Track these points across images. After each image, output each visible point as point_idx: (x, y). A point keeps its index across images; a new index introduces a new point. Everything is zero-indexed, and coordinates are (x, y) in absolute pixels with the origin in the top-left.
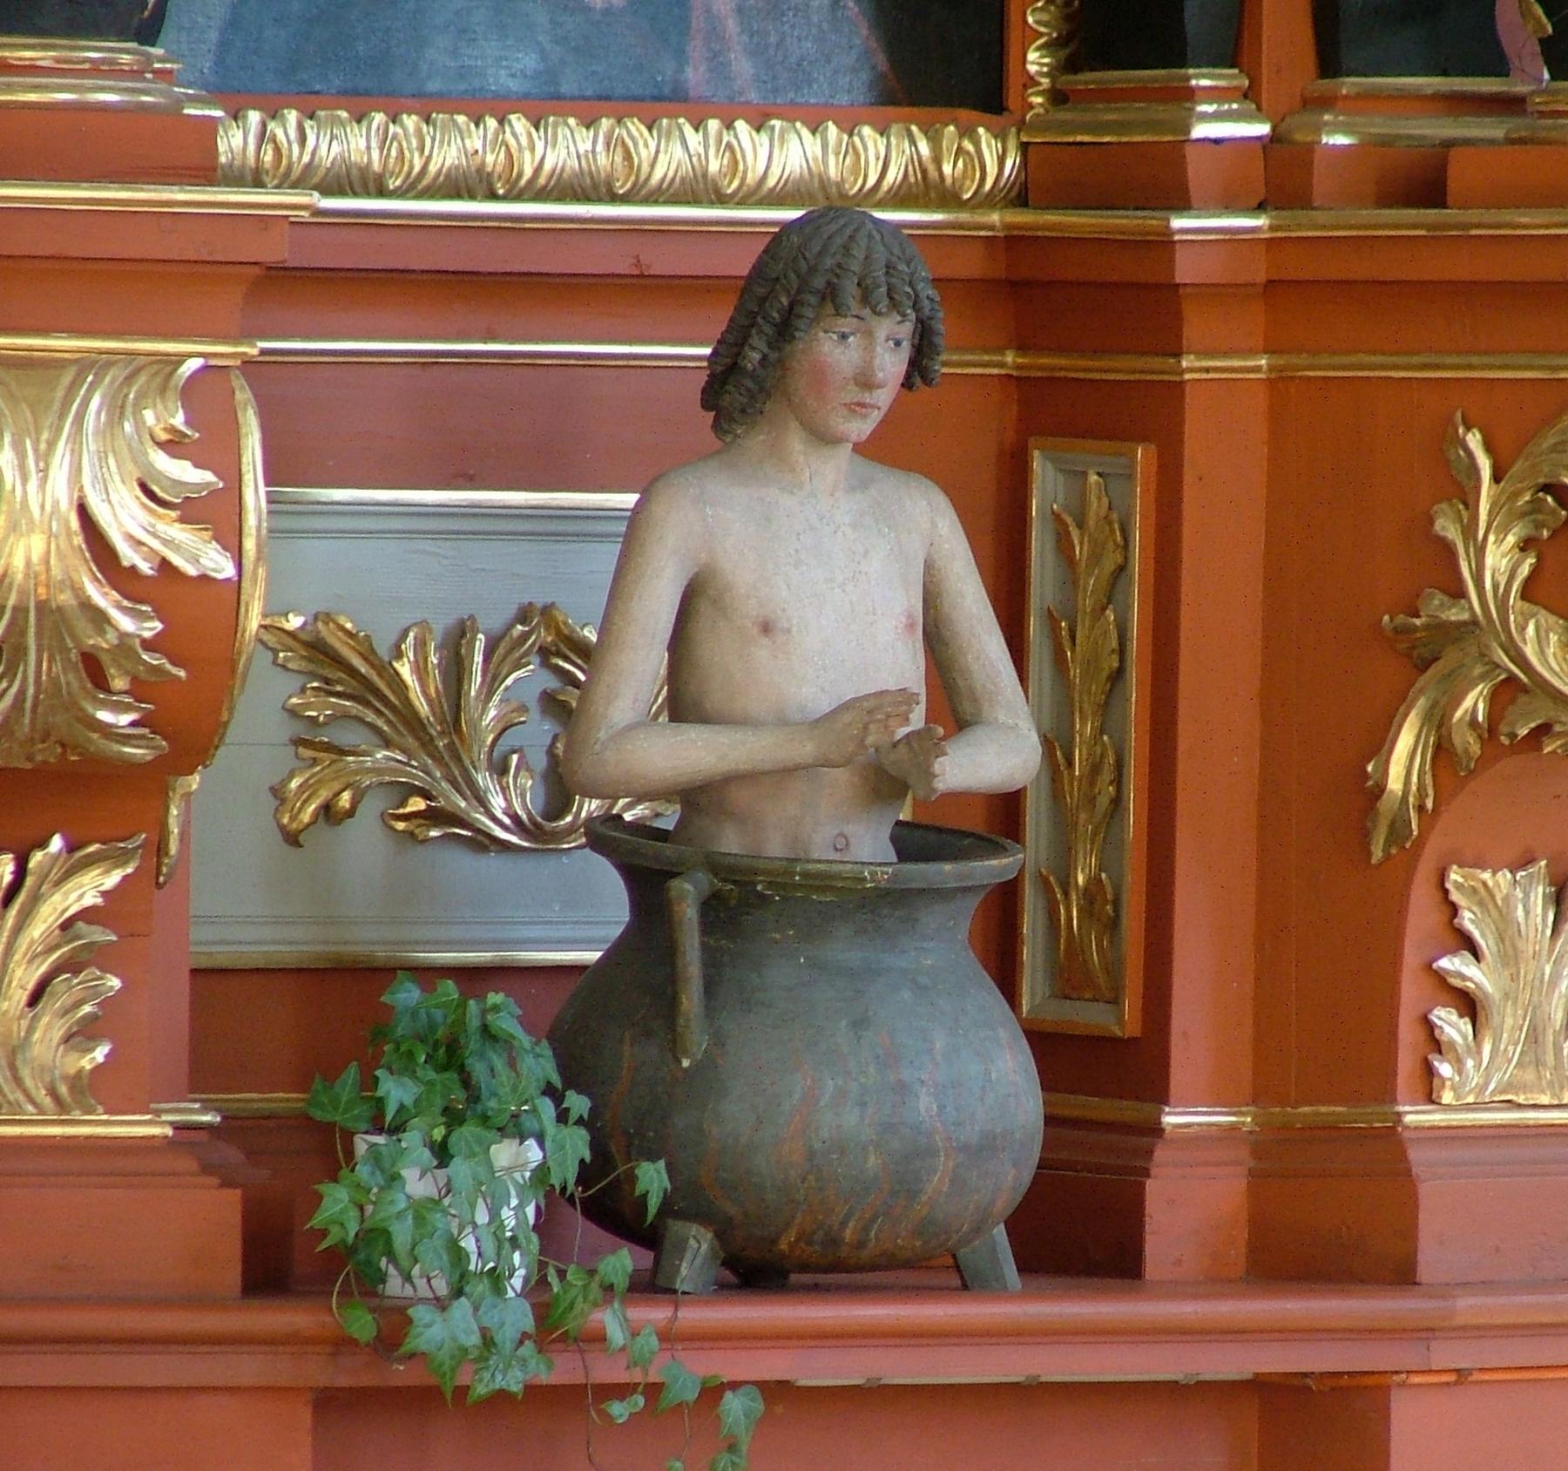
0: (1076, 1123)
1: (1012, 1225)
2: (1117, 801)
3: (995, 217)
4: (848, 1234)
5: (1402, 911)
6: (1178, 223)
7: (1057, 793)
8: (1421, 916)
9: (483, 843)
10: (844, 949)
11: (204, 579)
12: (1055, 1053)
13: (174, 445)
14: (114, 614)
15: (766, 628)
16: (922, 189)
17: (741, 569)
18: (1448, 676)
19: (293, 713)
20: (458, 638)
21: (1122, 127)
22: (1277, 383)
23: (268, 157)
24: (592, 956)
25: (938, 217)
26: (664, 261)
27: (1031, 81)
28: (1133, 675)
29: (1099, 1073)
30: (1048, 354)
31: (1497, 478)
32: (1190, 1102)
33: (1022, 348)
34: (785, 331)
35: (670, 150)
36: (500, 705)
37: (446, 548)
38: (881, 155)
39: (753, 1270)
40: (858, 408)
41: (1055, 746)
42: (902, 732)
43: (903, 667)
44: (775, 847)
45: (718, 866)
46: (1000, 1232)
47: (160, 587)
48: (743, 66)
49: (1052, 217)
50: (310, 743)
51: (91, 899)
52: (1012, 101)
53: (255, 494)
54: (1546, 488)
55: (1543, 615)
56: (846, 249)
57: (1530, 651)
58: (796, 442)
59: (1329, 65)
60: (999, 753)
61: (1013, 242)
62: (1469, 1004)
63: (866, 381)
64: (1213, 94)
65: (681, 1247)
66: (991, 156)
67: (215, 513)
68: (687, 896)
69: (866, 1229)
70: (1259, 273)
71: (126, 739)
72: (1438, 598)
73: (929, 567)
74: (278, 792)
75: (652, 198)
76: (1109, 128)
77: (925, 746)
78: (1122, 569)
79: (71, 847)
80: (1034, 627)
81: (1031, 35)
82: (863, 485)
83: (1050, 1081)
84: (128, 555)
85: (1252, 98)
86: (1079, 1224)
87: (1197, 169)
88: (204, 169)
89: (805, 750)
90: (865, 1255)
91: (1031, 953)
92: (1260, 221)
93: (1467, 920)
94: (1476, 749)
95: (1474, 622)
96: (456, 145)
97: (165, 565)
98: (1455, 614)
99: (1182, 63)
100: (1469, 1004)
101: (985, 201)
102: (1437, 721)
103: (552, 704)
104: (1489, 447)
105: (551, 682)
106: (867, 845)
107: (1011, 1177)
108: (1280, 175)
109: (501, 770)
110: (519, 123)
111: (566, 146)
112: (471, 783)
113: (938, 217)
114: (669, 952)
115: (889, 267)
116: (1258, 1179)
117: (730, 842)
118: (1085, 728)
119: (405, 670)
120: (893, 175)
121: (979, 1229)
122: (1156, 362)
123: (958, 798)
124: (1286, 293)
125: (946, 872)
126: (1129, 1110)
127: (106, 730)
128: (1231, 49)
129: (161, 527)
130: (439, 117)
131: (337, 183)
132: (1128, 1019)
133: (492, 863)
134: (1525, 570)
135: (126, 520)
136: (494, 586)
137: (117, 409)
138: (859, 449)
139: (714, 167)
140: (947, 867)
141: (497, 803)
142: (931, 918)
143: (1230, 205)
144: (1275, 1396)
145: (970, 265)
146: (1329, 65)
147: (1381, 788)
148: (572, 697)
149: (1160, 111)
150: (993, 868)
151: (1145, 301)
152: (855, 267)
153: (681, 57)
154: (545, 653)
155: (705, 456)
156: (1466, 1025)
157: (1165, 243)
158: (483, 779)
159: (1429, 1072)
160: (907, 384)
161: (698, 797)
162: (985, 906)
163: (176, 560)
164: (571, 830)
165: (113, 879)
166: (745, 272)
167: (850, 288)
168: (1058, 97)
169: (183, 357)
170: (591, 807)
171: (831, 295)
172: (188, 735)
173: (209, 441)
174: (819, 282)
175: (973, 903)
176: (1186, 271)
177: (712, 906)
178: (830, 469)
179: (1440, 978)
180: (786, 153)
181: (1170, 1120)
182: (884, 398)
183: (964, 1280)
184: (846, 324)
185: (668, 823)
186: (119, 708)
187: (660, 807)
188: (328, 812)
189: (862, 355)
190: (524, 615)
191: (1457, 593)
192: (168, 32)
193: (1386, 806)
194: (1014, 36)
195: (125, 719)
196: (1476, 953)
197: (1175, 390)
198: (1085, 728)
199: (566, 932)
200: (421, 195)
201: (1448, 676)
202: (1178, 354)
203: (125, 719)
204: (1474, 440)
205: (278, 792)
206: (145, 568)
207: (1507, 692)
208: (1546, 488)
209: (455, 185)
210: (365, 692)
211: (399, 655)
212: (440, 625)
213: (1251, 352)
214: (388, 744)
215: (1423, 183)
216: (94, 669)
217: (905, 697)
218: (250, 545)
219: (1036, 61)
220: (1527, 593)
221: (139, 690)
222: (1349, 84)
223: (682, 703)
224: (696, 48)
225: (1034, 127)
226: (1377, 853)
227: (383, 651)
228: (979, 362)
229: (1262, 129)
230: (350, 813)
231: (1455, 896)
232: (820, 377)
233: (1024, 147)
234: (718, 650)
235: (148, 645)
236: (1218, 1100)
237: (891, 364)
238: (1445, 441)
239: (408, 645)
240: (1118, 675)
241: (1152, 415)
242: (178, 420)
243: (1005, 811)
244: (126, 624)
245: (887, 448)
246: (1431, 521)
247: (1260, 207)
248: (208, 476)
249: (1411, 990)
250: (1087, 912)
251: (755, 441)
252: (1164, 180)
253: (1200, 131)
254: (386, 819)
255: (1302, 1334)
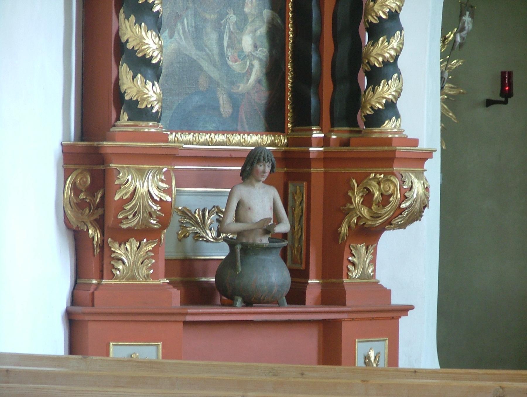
0: (294, 282)
1: (287, 297)
2: (302, 234)
3: (283, 148)
4: (262, 298)
5: (343, 263)
6: (311, 149)
7: (293, 234)
8: (346, 249)
9: (208, 241)
10: (262, 257)
11: (167, 201)
12: (293, 272)
13: (162, 181)
14: (153, 206)
15: (249, 209)
16: (272, 144)
17: (246, 200)
18: (350, 216)
19: (180, 222)
20: (204, 211)
21: (299, 135)
22: (325, 173)
23: (176, 140)
24: (224, 257)
25: (275, 148)
26: (234, 155)
27: (289, 128)
28: (304, 216)
29: (299, 275)
30: (290, 170)
31: (358, 186)
32: (312, 279)
33: (287, 168)
34: (252, 164)
35: (237, 138)
36: (211, 220)
37: (202, 197)
38: (267, 139)
39: (248, 303)
40: (263, 176)
41: (292, 226)
42: (270, 224)
43: (269, 214)
44: (251, 241)
45: (242, 244)
46: (284, 298)
47: (161, 202)
48: (246, 127)
49: (292, 148)
50: (183, 226)
51: (150, 249)
52: (286, 131)
53: (174, 189)
54: (365, 188)
55: (364, 207)
56: (261, 153)
57: (362, 212)
58: (254, 181)
59: (333, 126)
60: (284, 227)
61: (285, 152)
62: (353, 264)
63: (264, 172)
64: (315, 130)
65: (237, 300)
66: (284, 140)
67: (168, 191)
68: (239, 247)
69: (264, 297)
70: (322, 157)
71: (155, 225)
72: (349, 204)
73: (274, 200)
74: (178, 233)
75: (233, 145)
76: (296, 135)
77: (273, 226)
78: (302, 200)
79: (147, 241)
80: (289, 209)
81: (288, 122)
82: (264, 187)
83: (292, 276)
84: (155, 198)
85: (321, 131)
86: (296, 296)
87: (313, 142)
88: (167, 141)
89: (255, 227)
90: (265, 301)
91: (289, 257)
92: (322, 149)
93: (353, 252)
94: (354, 227)
95: (354, 208)
96: (204, 138)
97: (161, 199)
98: (352, 207)
99: (311, 126)
100: (353, 264)
101: (282, 146)
102: (349, 222)
103: (218, 220)
104: (356, 182)
105: (218, 217)
106: (265, 240)
107: (287, 290)
108: (325, 142)
109: (210, 230)
110: (213, 134)
111: (220, 138)
112: (206, 232)
113: (275, 148)
114: (236, 257)
115: (268, 156)
116: (323, 286)
117: (244, 241)
118: (297, 224)
119: (196, 215)
120: (268, 142)
121: (282, 297)
122: (307, 170)
123: (278, 234)
124: (326, 159)
125: (276, 244)
126: (303, 280)
127: (152, 223)
128: (319, 123)
129: (160, 193)
130: (201, 134)
131: (204, 144)
132: (303, 267)
133: (209, 244)
134: (362, 200)
135: (155, 192)
136: (209, 203)
137: (154, 176)
138: (263, 182)
139: (242, 141)
140: (277, 244)
141: (210, 235)
142: (274, 251)
143: (318, 146)
144: (324, 323)
145: (279, 156)
146: (333, 126)
147: (340, 233)
148: (221, 219)
149: (308, 133)
150: (285, 243)
151: (305, 160)
152: (263, 155)
153: (237, 125)
154: (217, 213)
155: (241, 184)
156: (353, 268)
157: (308, 152)
158: (208, 231)
159: (348, 274)
160: (270, 172)
161: (240, 234)
162: (282, 250)
163: (162, 198)
164: (221, 239)
165: (153, 246)
166: (246, 156)
167: (262, 158)
168: (292, 131)
169: (163, 168)
170: (224, 235)
171: (259, 161)
172: (164, 223)
173: (168, 181)
174: (257, 158)
175: (280, 249)
176: (312, 156)
177: (242, 250)
178: (261, 184)
179: (349, 261)
180: (253, 139)
181: (310, 281)
182: (267, 175)
183: (278, 304)
184: (262, 164)
185: (235, 238)
186: (154, 220)
187: (234, 235)
188: (185, 236)
189: (265, 168)
190: (214, 207)
191: (352, 203)
192: (162, 121)
193: (341, 235)
194: (286, 121)
195: (155, 222)
196: (355, 257)
197: (310, 173)
198: (297, 224)
199: (220, 254)
200: (199, 145)
201: (350, 216)
202: (310, 168)
203: (155, 222)
204: (354, 181)
205: (178, 233)
206: (158, 199)
207: (359, 218)
208: (365, 188)
209: (204, 144)
210: (190, 218)
211: (195, 213)
212: (201, 209)
213: (321, 168)
214: (194, 226)
215: (346, 143)
216: (150, 215)
217: (270, 219)
218: (173, 196)
219: (289, 125)
220: (362, 203)
221: (157, 217)
222: (336, 129)
223: (238, 219)
224: (239, 123)
225: (289, 135)
226: (340, 242)
227: (193, 212)
228: (280, 170)
229: (323, 135)
230: (188, 236)
231: (352, 248)
232: (257, 171)
233: (288, 138)
234: (242, 212)
235: (158, 211)
236: (317, 278)
237: (268, 170)
238: (349, 181)
239: (197, 211)
240: (302, 216)
241: (307, 177)
242: (163, 178)
243: (284, 236)
244: (155, 208)
245: (268, 182)
246: (348, 193)
247: (322, 147)
248: (167, 186)
249: (345, 262)
250: (298, 251)
251: (248, 181)
252: (308, 142)
253: (314, 136)
254: (193, 237)
255: (329, 313)
